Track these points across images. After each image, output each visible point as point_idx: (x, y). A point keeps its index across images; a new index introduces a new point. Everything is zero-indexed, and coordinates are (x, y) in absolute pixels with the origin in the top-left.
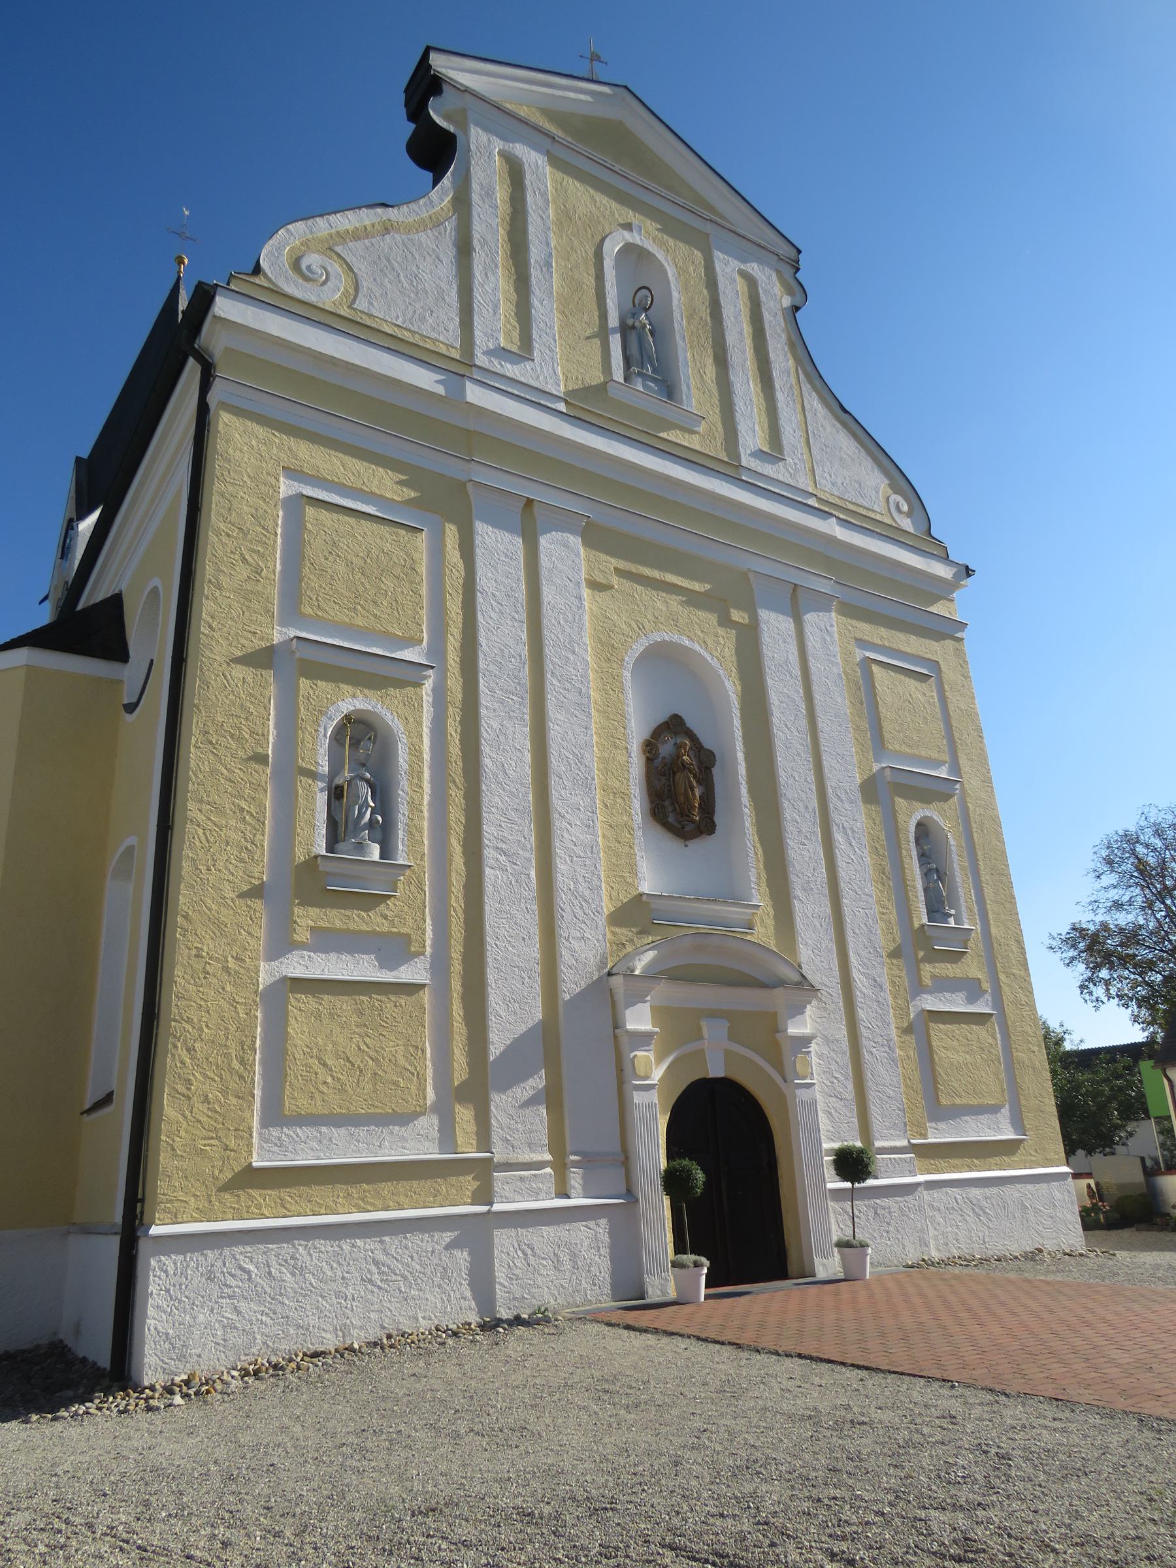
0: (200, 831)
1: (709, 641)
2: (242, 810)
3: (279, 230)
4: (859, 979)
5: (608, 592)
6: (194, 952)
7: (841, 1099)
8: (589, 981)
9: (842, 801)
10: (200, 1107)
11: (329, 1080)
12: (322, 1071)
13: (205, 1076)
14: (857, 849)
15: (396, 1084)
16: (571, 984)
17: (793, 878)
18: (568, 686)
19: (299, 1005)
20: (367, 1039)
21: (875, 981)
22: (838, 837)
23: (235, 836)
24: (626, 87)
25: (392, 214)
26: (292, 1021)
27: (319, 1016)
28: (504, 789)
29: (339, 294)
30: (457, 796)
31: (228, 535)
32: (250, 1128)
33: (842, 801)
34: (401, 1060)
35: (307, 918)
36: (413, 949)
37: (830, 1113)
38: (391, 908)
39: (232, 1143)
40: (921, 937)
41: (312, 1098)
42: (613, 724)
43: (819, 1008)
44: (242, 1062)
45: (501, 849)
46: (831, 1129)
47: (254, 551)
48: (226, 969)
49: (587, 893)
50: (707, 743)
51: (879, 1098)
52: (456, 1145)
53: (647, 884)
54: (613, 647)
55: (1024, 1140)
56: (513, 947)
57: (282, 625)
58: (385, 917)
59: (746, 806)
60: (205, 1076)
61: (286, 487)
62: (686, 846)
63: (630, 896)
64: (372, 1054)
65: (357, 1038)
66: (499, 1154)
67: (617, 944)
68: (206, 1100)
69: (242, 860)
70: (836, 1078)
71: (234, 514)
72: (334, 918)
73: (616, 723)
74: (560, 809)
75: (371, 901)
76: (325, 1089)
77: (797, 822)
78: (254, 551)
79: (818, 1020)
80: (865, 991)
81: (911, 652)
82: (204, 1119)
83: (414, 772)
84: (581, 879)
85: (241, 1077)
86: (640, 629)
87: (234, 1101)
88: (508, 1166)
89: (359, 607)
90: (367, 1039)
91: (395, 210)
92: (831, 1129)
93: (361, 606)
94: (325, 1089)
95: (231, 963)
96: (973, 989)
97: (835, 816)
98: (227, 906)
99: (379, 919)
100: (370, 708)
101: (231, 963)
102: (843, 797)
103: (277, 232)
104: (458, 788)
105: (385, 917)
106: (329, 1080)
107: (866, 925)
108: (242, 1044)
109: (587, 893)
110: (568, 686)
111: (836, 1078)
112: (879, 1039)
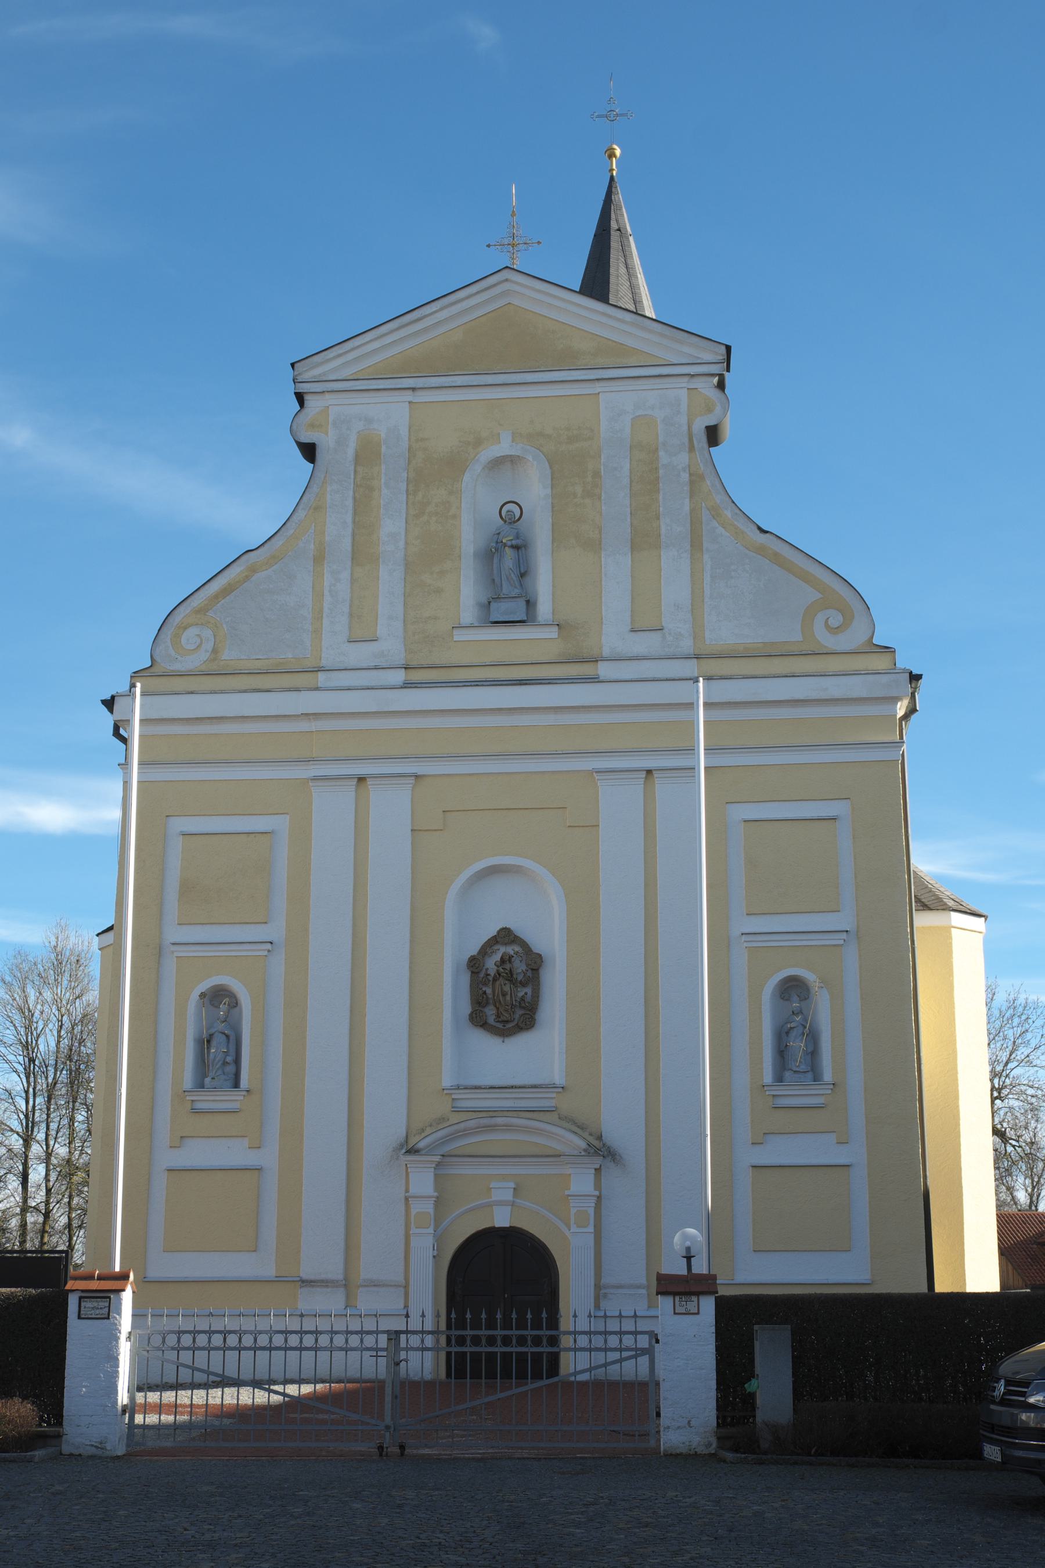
62: (503, 1042)
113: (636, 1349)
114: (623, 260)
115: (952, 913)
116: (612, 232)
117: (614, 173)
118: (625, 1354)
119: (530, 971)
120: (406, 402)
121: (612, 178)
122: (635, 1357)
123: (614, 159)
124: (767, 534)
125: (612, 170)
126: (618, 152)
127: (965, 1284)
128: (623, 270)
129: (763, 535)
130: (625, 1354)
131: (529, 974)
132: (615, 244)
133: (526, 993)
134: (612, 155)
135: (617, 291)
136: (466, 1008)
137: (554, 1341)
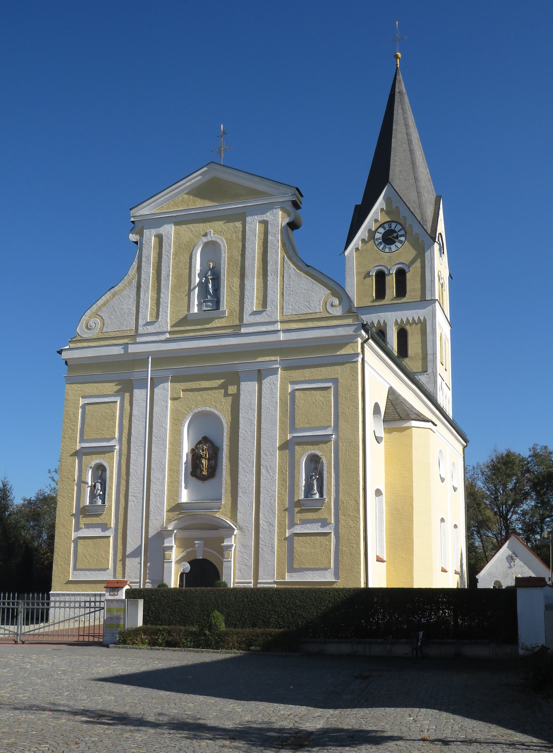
0: (60, 503)
1: (217, 405)
2: (69, 496)
3: (83, 316)
4: (263, 523)
5: (179, 400)
6: (59, 532)
7: (246, 566)
8: (157, 532)
9: (267, 455)
10: (60, 567)
11: (87, 561)
12: (85, 558)
13: (61, 560)
14: (271, 474)
15: (102, 561)
16: (152, 533)
17: (239, 489)
18: (159, 439)
19: (81, 542)
20: (96, 551)
21: (270, 524)
22: (263, 471)
23: (67, 503)
24: (212, 162)
25: (116, 288)
26: (79, 547)
27: (85, 546)
28: (136, 478)
29: (98, 330)
30: (123, 482)
31: (67, 422)
32: (70, 572)
33: (267, 455)
34: (103, 555)
35: (83, 521)
36: (108, 527)
37: (241, 570)
38: (102, 517)
39: (66, 575)
40: (299, 503)
41: (83, 565)
42: (176, 448)
43: (242, 535)
44: (68, 557)
45: (134, 496)
46: (240, 575)
47: (73, 425)
48: (65, 536)
49: (159, 505)
50: (217, 444)
51: (264, 565)
52: (116, 577)
53: (185, 497)
54: (179, 420)
55: (337, 582)
56: (135, 524)
57: (290, 433)
58: (101, 519)
59: (224, 466)
60: (61, 560)
61: (81, 402)
62: (203, 483)
63: (175, 504)
64: (97, 554)
65: (93, 550)
66: (86, 609)
67: (169, 520)
68: (61, 565)
69: (69, 509)
70: (245, 558)
71: (69, 416)
72: (89, 520)
73: (177, 447)
74: (153, 481)
75: (98, 515)
76: (86, 563)
77: (244, 468)
78: (73, 425)
79: (241, 539)
80: (265, 528)
81: (321, 378)
82: (61, 569)
83: (111, 478)
84: (158, 502)
85: (68, 560)
86: (190, 410)
87: (66, 565)
88: (85, 617)
89: (98, 433)
90: (96, 551)
91: (117, 287)
92: (240, 575)
93: (99, 432)
94: (86, 563)
95: (66, 534)
96: (325, 523)
97: (262, 462)
98: (65, 521)
99: (100, 520)
100: (100, 462)
101: (66, 534)
102: (268, 454)
103: (82, 318)
104: (123, 480)
105: (101, 519)
106: (87, 561)
107: (270, 503)
108: (68, 553)
109: (159, 505)
110: (159, 439)
111: (245, 558)
112: (268, 545)
113: (100, 607)
114: (401, 106)
115: (412, 421)
116: (396, 94)
117: (398, 66)
118: (97, 609)
119: (214, 454)
120: (294, 187)
121: (397, 68)
122: (100, 610)
123: (398, 59)
124: (310, 267)
125: (397, 65)
126: (399, 54)
127: (413, 582)
128: (400, 111)
129: (308, 268)
130: (97, 609)
131: (214, 455)
132: (397, 100)
133: (212, 463)
134: (396, 57)
135: (397, 121)
136: (190, 470)
137: (48, 604)
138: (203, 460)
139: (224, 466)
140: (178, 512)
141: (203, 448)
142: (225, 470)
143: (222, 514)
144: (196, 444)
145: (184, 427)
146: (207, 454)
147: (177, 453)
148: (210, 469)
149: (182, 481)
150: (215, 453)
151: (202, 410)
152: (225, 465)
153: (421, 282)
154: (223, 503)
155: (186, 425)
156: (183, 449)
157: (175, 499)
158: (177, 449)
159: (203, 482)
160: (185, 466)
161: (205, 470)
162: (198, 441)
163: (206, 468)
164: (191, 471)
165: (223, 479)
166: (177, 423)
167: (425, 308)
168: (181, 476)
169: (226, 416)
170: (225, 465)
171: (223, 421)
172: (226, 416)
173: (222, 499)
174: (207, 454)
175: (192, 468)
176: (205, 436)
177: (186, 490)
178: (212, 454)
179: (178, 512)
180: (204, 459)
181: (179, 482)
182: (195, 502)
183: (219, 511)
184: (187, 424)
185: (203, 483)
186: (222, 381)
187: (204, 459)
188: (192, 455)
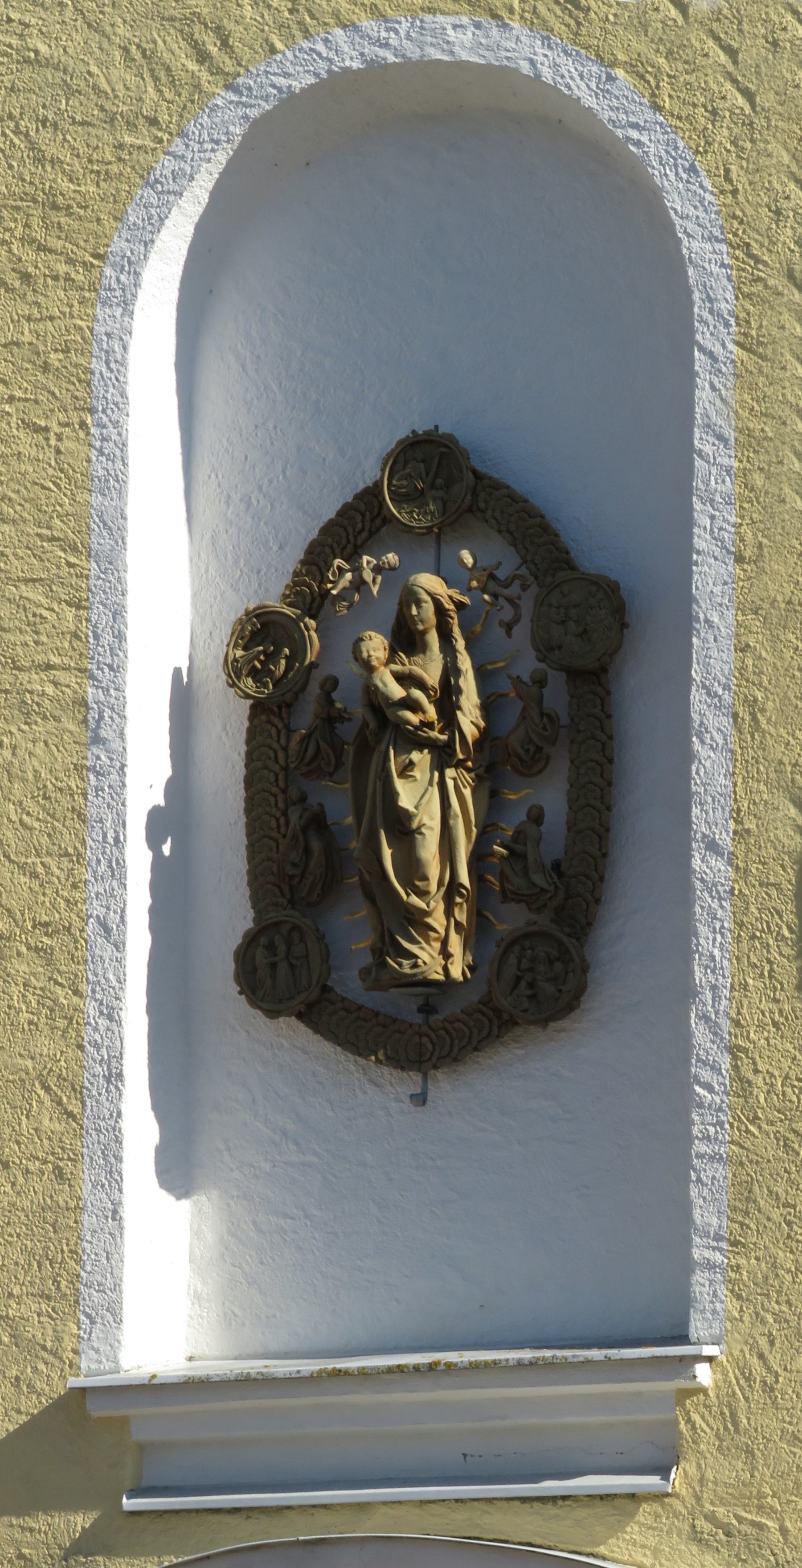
42: (20, 604)
59: (712, 846)
63: (32, 1406)
73: (34, 594)
86: (203, 57)
133: (537, 817)
138: (406, 770)
139: (712, 846)
140: (81, 1521)
141: (410, 597)
142: (725, 914)
143: (696, 1537)
144: (296, 553)
145: (127, 305)
146: (468, 684)
147: (35, 681)
148: (506, 896)
149: (114, 1077)
150: (574, 675)
151: (375, 67)
152: (725, 840)
153: (250, 884)
154: (704, 1374)
155: (144, 299)
156: (118, 613)
157: (33, 1331)
158: (35, 624)
159: (412, 1081)
160: (159, 865)
161: (438, 921)
162: (329, 512)
163: (452, 889)
164: (251, 941)
165: (700, 1034)
166: (28, 255)
167: (397, 794)
168: (112, 1015)
169: (722, 136)
170: (725, 840)
171: (674, 202)
172: (722, 136)
173: (697, 1327)
174: (468, 684)
175: (257, 898)
176: (403, 433)
177: (185, 1204)
178: (540, 682)
179: (81, 1521)
180: (421, 758)
181: (78, 1091)
182: (309, 1366)
183: (659, 1497)
184: (176, 270)
185: (420, 1099)
186: (169, 840)
187: (421, 758)
188: (258, 708)
